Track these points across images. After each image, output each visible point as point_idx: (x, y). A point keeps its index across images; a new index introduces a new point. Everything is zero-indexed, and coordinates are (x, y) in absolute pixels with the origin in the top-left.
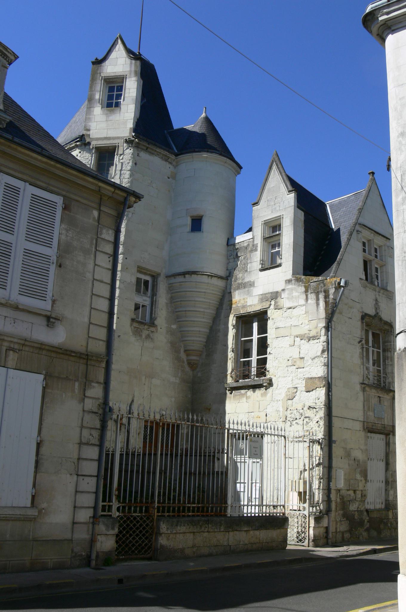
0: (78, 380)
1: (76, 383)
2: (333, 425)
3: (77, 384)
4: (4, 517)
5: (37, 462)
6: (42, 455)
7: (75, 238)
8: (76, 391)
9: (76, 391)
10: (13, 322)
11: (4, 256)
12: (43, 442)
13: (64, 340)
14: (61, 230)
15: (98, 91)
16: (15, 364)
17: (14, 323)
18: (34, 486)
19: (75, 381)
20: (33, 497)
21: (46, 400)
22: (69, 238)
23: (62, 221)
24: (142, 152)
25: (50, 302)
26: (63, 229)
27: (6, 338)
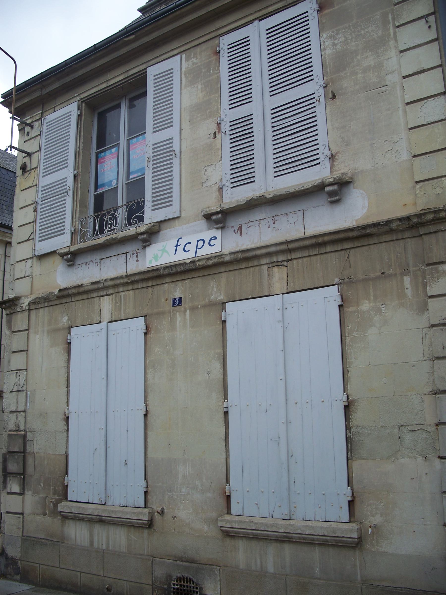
0: (407, 272)
1: (405, 278)
2: (29, 585)
3: (407, 280)
4: (300, 538)
5: (348, 440)
6: (357, 427)
7: (350, 38)
8: (409, 293)
9: (409, 293)
10: (272, 222)
11: (246, 128)
12: (356, 404)
13: (365, 211)
14: (322, 44)
15: (152, 284)
16: (286, 284)
17: (274, 223)
18: (350, 483)
19: (402, 275)
20: (351, 503)
21: (349, 327)
22: (339, 46)
23: (320, 31)
24: (147, 377)
25: (327, 163)
26: (325, 40)
27: (81, 519)
